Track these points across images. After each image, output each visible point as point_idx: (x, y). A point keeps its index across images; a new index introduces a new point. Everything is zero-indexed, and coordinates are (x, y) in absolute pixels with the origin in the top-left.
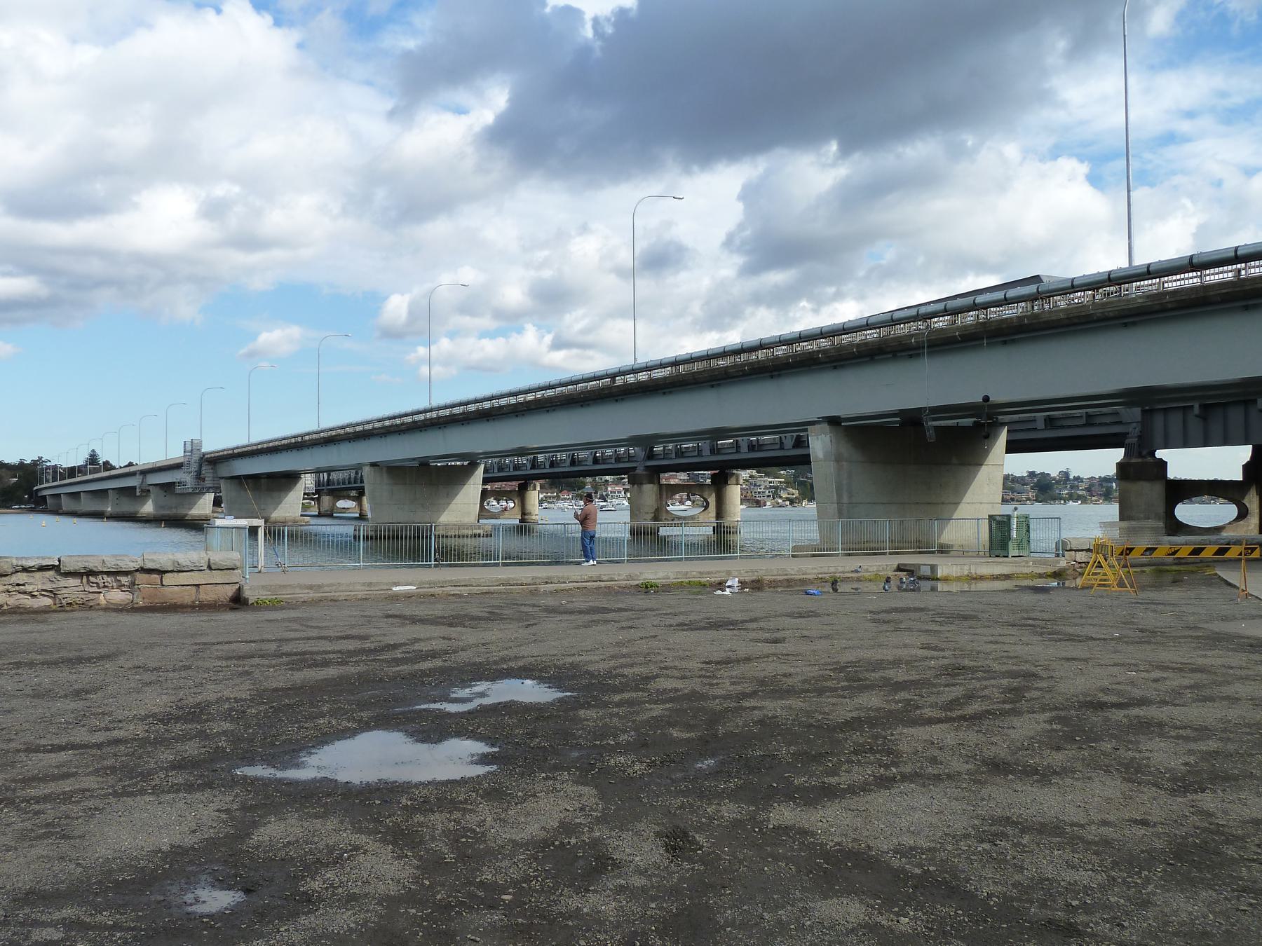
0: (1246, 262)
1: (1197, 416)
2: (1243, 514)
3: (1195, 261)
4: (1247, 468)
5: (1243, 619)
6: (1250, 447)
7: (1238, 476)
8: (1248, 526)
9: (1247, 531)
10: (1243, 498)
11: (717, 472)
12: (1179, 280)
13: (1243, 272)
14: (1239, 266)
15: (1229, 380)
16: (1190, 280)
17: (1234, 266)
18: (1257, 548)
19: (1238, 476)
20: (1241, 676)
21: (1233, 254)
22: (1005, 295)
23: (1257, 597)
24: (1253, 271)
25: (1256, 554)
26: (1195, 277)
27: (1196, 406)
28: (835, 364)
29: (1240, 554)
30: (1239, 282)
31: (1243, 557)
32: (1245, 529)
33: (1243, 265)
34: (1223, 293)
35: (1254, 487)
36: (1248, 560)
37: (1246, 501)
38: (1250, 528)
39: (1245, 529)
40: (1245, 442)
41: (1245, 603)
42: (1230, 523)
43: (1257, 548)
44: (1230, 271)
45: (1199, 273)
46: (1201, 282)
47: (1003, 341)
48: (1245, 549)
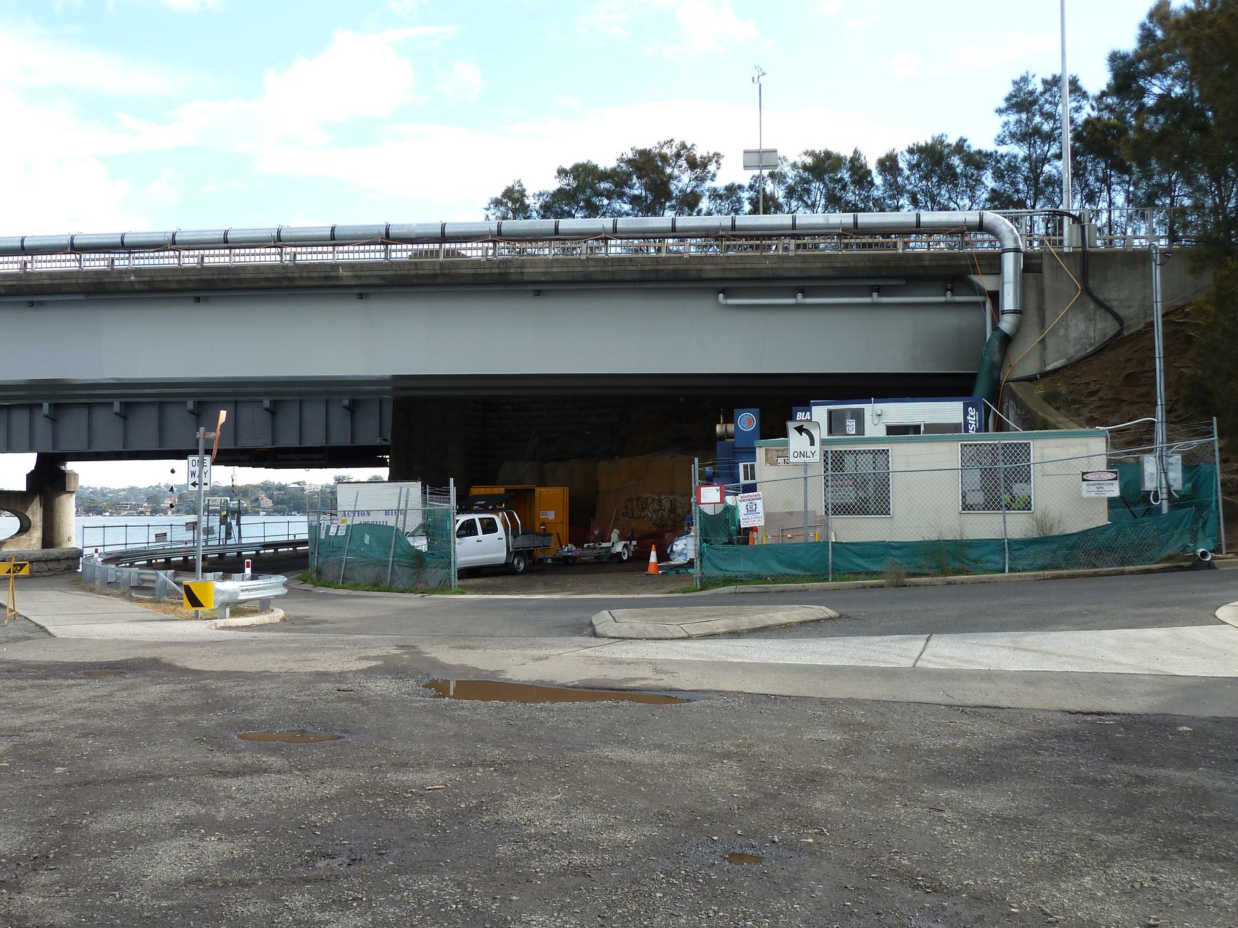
0: (32, 255)
1: (46, 416)
2: (25, 528)
3: (126, 240)
4: (31, 477)
5: (6, 642)
6: (35, 455)
7: (22, 486)
8: (31, 540)
9: (29, 545)
10: (26, 511)
11: (452, 480)
12: (162, 258)
13: (29, 265)
14: (25, 258)
15: (375, 377)
16: (324, 256)
17: (20, 258)
18: (25, 564)
19: (22, 486)
20: (939, 768)
21: (120, 240)
22: (733, 221)
23: (26, 618)
24: (39, 265)
25: (25, 571)
26: (172, 257)
27: (46, 406)
28: (197, 295)
29: (9, 572)
30: (24, 276)
31: (12, 574)
32: (27, 543)
33: (30, 257)
34: (8, 286)
35: (38, 497)
36: (16, 577)
37: (29, 514)
38: (33, 542)
39: (27, 543)
40: (30, 450)
41: (12, 625)
42: (11, 537)
43: (25, 564)
44: (16, 263)
45: (78, 256)
46: (80, 267)
47: (28, 302)
48: (14, 565)
